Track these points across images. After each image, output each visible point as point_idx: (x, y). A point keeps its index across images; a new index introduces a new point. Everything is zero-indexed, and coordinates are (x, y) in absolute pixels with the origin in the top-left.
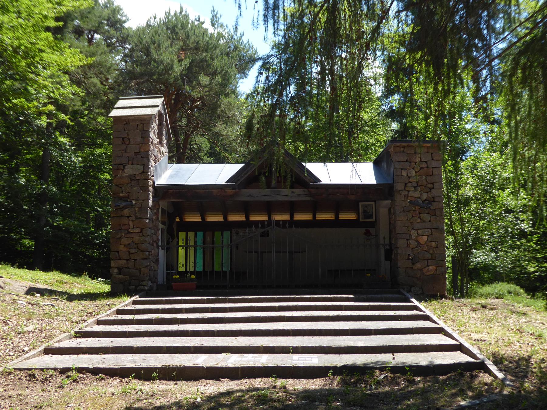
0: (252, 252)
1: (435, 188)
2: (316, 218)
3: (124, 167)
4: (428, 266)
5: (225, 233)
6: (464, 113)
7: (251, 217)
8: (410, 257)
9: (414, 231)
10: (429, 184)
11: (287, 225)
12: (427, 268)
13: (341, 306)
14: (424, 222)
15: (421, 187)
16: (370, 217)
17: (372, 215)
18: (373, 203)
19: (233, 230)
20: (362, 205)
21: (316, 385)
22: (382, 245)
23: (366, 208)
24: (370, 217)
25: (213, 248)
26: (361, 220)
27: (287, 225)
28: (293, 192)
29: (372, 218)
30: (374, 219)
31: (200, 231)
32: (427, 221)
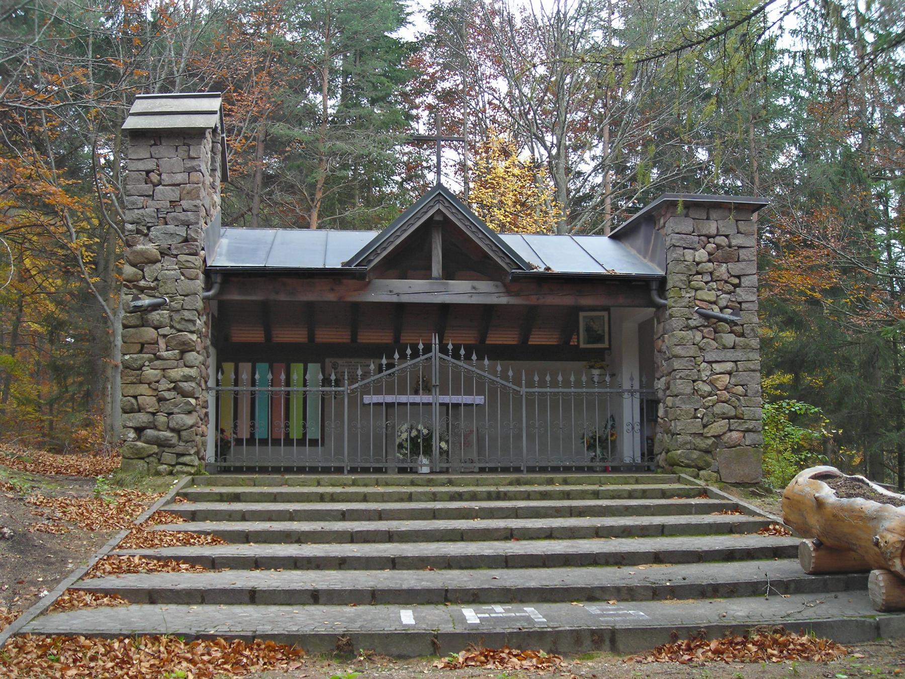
0: (236, 393)
1: (743, 285)
2: (528, 341)
3: (149, 228)
4: (730, 430)
5: (258, 365)
6: (611, 172)
7: (359, 337)
8: (699, 415)
9: (704, 364)
10: (732, 278)
11: (462, 352)
12: (729, 434)
13: (647, 507)
14: (725, 347)
15: (718, 282)
16: (599, 339)
17: (604, 336)
18: (605, 314)
19: (327, 360)
20: (584, 317)
21: (98, 497)
22: (629, 391)
23: (592, 323)
24: (599, 339)
25: (288, 393)
26: (582, 346)
27: (462, 352)
28: (474, 288)
29: (603, 342)
30: (606, 345)
31: (262, 361)
32: (729, 346)
